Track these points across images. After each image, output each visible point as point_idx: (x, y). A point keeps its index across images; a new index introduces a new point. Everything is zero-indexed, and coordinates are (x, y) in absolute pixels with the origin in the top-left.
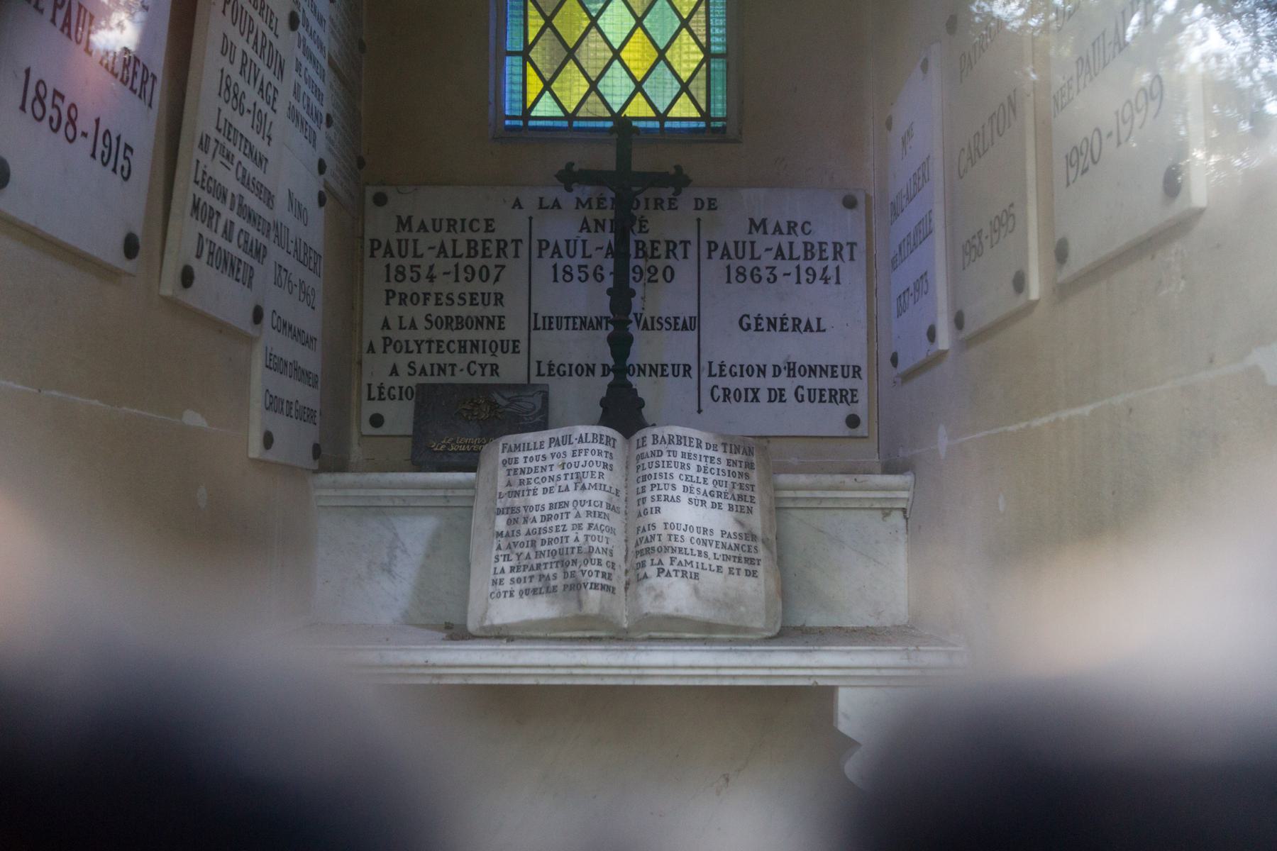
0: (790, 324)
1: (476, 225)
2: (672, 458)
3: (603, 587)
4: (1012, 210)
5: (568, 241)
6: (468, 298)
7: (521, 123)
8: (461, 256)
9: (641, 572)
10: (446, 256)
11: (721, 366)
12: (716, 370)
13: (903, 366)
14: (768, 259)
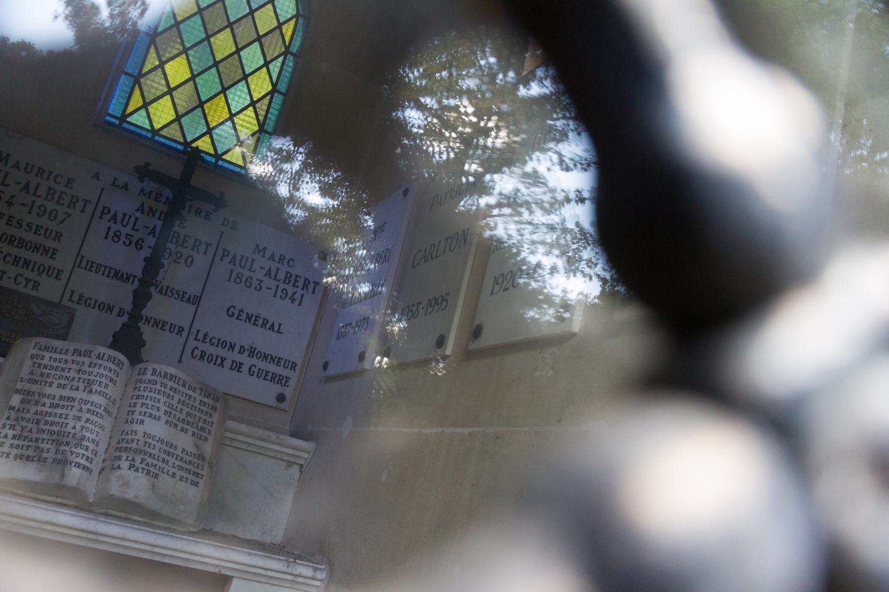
0: (260, 322)
1: (59, 179)
2: (163, 389)
3: (84, 467)
4: (447, 297)
5: (125, 215)
6: (34, 227)
7: (117, 122)
8: (39, 196)
9: (117, 464)
10: (28, 192)
11: (205, 335)
12: (201, 336)
13: (331, 371)
14: (260, 274)
